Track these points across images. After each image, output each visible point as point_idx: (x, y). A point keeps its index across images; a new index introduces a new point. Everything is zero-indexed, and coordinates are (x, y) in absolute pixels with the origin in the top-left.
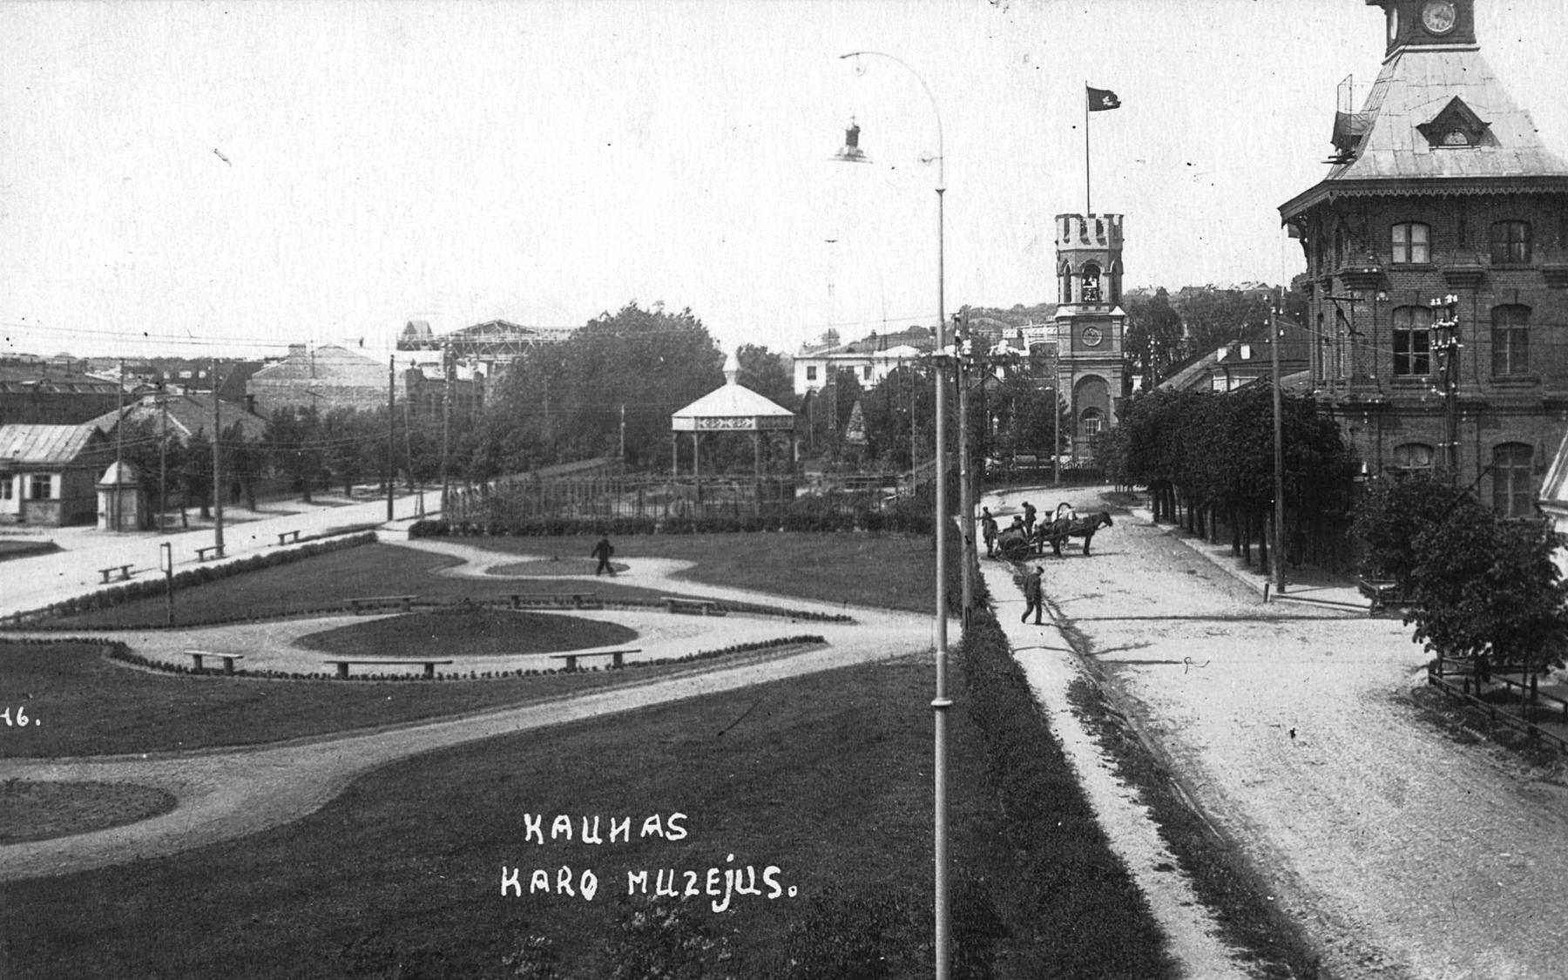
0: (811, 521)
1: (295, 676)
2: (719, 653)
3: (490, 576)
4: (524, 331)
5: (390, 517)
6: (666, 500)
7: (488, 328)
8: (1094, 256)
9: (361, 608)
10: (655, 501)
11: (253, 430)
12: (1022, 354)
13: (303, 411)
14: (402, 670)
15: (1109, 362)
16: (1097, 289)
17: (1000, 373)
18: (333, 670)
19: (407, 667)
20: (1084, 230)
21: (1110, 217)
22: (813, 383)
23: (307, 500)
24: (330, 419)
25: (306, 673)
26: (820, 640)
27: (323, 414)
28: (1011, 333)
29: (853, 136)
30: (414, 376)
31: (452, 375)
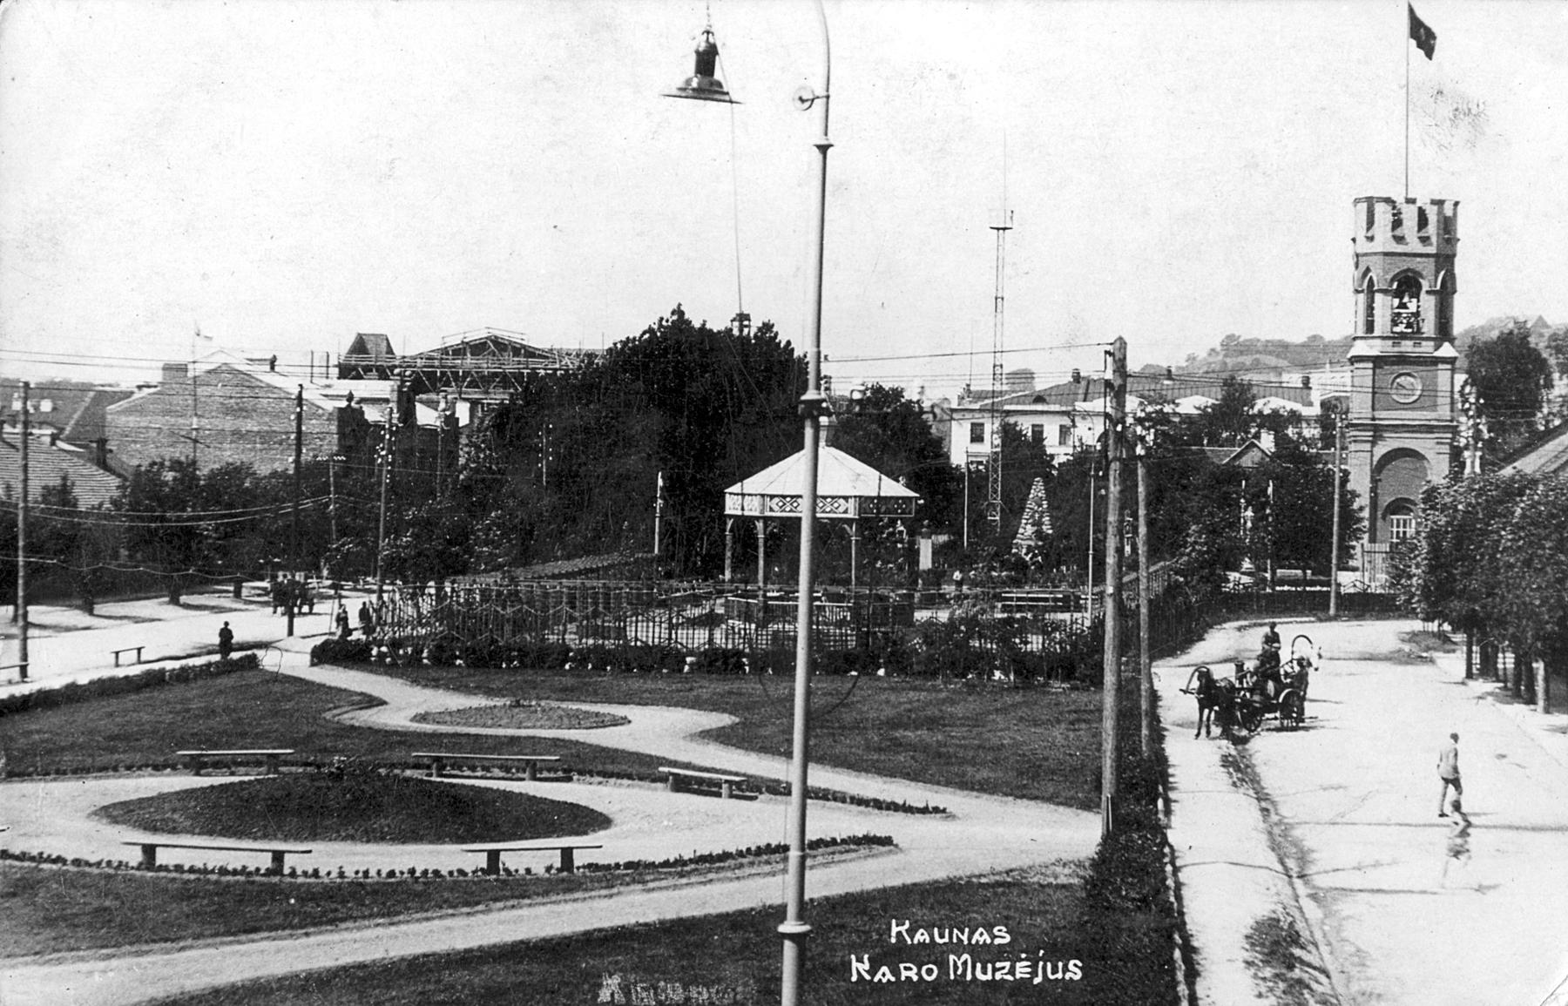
0: (954, 657)
1: (77, 862)
2: (725, 856)
3: (415, 726)
4: (531, 353)
5: (291, 633)
6: (711, 621)
7: (478, 348)
8: (1416, 265)
9: (205, 765)
10: (694, 623)
11: (95, 491)
12: (1306, 411)
13: (176, 465)
14: (234, 861)
15: (1430, 429)
16: (1417, 314)
17: (1267, 442)
18: (135, 856)
19: (245, 855)
20: (1397, 223)
21: (1439, 203)
22: (976, 448)
23: (175, 601)
24: (213, 475)
25: (93, 860)
26: (887, 841)
27: (203, 472)
28: (1294, 379)
29: (706, 60)
30: (350, 419)
31: (408, 414)
